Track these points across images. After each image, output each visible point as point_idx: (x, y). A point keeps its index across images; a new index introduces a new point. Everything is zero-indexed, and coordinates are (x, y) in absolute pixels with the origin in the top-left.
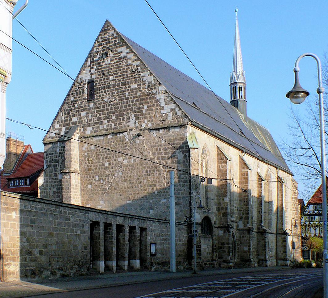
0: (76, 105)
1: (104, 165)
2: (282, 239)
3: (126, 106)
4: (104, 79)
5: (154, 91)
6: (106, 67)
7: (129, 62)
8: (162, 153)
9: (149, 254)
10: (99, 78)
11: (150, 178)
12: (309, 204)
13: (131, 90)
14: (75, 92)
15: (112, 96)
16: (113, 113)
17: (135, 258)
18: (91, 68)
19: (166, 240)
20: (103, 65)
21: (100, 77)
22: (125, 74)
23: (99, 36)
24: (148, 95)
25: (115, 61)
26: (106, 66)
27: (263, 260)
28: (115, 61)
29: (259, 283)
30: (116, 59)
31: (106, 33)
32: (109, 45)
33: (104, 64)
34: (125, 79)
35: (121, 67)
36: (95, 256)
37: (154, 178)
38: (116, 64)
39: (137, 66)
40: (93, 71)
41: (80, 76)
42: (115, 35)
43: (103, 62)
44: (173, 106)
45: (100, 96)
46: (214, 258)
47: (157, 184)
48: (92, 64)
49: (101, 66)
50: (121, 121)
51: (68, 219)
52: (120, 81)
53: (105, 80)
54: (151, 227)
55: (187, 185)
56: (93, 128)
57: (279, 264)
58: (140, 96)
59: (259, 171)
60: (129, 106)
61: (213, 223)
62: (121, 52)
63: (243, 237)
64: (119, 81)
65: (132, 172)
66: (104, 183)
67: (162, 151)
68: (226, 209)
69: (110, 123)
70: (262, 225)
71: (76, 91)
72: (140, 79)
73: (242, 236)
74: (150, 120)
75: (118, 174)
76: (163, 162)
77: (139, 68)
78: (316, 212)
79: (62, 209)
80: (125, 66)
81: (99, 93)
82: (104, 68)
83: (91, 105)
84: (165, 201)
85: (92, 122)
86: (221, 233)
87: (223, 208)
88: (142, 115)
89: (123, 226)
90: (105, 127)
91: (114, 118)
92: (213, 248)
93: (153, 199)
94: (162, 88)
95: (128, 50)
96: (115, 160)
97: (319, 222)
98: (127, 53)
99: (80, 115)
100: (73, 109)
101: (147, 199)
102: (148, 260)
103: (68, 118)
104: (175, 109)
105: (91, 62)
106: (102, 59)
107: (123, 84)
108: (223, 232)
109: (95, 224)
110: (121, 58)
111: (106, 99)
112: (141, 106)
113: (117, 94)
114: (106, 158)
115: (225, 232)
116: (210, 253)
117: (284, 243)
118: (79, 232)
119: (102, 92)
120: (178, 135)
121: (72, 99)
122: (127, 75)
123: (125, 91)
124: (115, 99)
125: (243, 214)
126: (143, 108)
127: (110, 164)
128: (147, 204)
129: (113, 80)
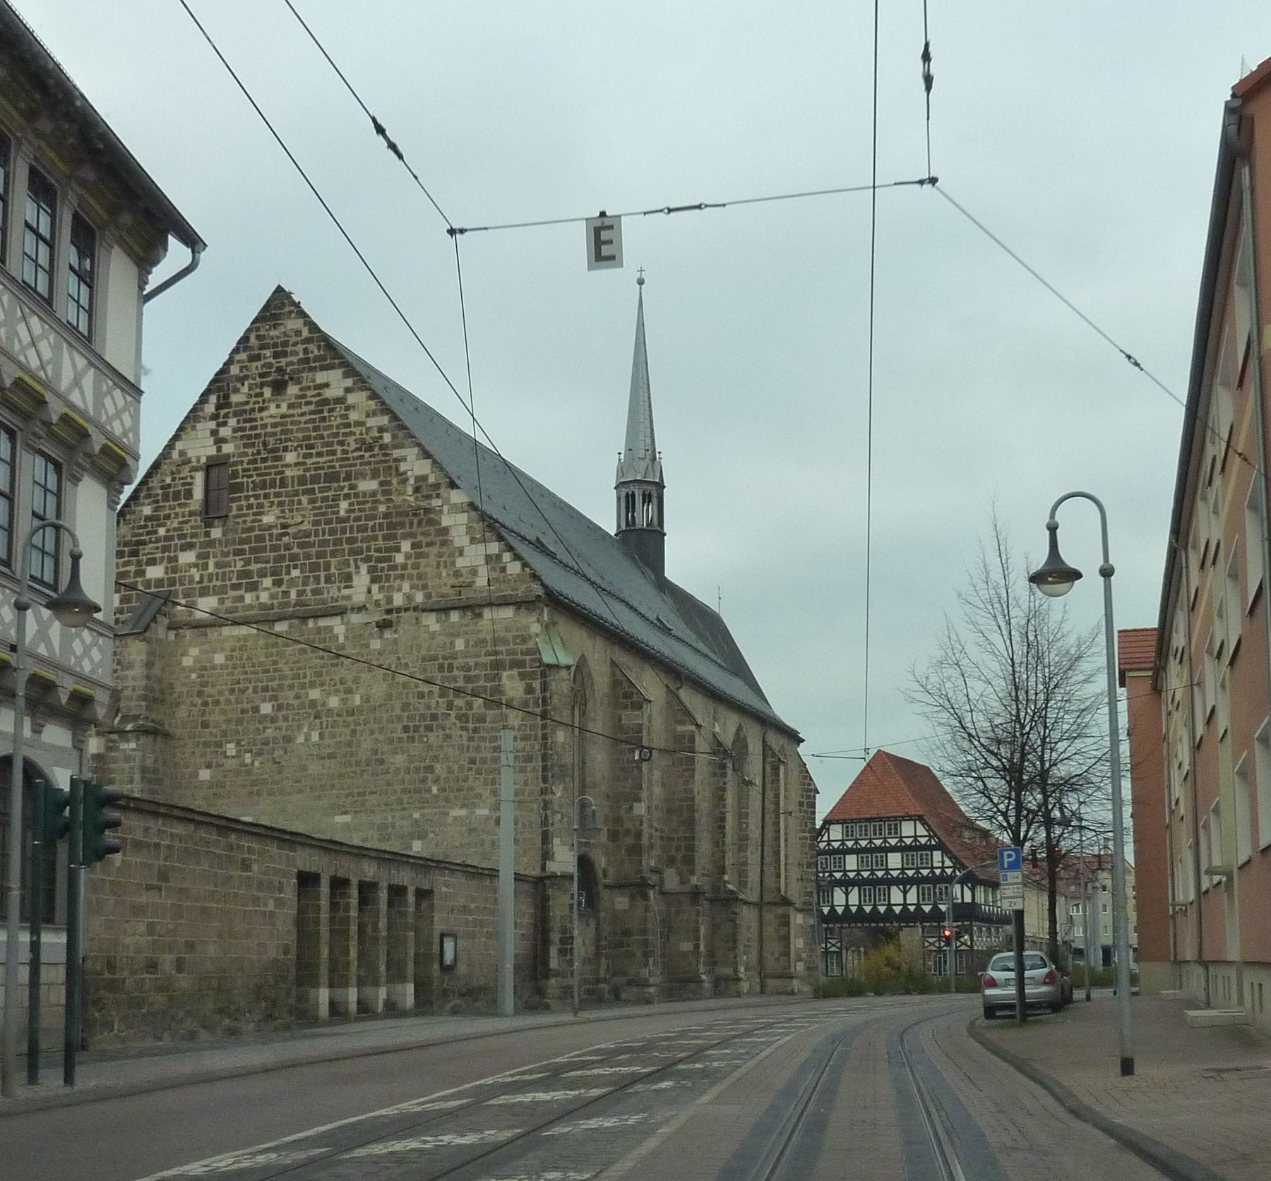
0: (162, 532)
1: (256, 709)
2: (776, 917)
3: (338, 542)
4: (264, 460)
5: (436, 503)
6: (275, 425)
7: (354, 416)
8: (455, 679)
9: (436, 966)
10: (246, 454)
11: (417, 749)
12: (827, 822)
13: (356, 495)
14: (160, 492)
15: (291, 511)
16: (294, 558)
17: (402, 979)
18: (219, 425)
19: (481, 924)
20: (262, 419)
21: (250, 451)
22: (339, 448)
23: (249, 330)
24: (415, 515)
25: (305, 409)
26: (273, 420)
27: (727, 979)
28: (305, 409)
29: (527, 1077)
30: (308, 403)
31: (275, 327)
32: (283, 361)
33: (264, 414)
34: (337, 464)
35: (326, 428)
36: (306, 974)
37: (430, 747)
38: (308, 417)
39: (381, 430)
40: (225, 432)
41: (179, 446)
42: (305, 333)
43: (261, 410)
44: (494, 547)
45: (250, 507)
46: (602, 974)
47: (438, 767)
48: (222, 412)
49: (255, 420)
50: (322, 584)
51: (246, 866)
52: (322, 468)
53: (269, 463)
54: (443, 885)
55: (534, 770)
56: (222, 601)
57: (768, 990)
58: (386, 516)
59: (717, 729)
60: (351, 541)
61: (600, 873)
62: (327, 385)
63: (678, 913)
64: (316, 469)
65: (354, 731)
66: (257, 764)
67: (456, 672)
68: (639, 835)
69: (284, 588)
70: (726, 877)
71: (162, 488)
72: (390, 467)
73: (673, 910)
74: (420, 583)
75: (308, 736)
76: (459, 702)
77: (387, 438)
78: (850, 844)
79: (233, 838)
80: (338, 427)
81: (247, 498)
82: (265, 426)
83: (216, 533)
84: (463, 812)
85: (219, 583)
86: (621, 902)
87: (627, 832)
88: (394, 568)
89: (406, 888)
90: (264, 597)
91: (295, 573)
92: (598, 947)
93: (423, 808)
94: (457, 497)
95: (349, 382)
96: (297, 697)
97: (903, 869)
98: (347, 390)
99: (176, 559)
100: (151, 542)
101: (404, 809)
102: (436, 983)
103: (132, 568)
104: (499, 557)
105: (219, 407)
106: (260, 399)
107: (333, 477)
108: (627, 900)
109: (307, 880)
110: (326, 402)
111: (268, 519)
112: (391, 543)
113: (310, 507)
114: (265, 689)
115: (632, 898)
116: (590, 960)
117: (783, 931)
118: (271, 906)
119: (256, 497)
120: (507, 629)
121: (147, 510)
122: (345, 452)
123: (336, 498)
124: (303, 519)
125: (678, 849)
126: (398, 550)
127: (280, 708)
128: (405, 823)
129: (297, 464)
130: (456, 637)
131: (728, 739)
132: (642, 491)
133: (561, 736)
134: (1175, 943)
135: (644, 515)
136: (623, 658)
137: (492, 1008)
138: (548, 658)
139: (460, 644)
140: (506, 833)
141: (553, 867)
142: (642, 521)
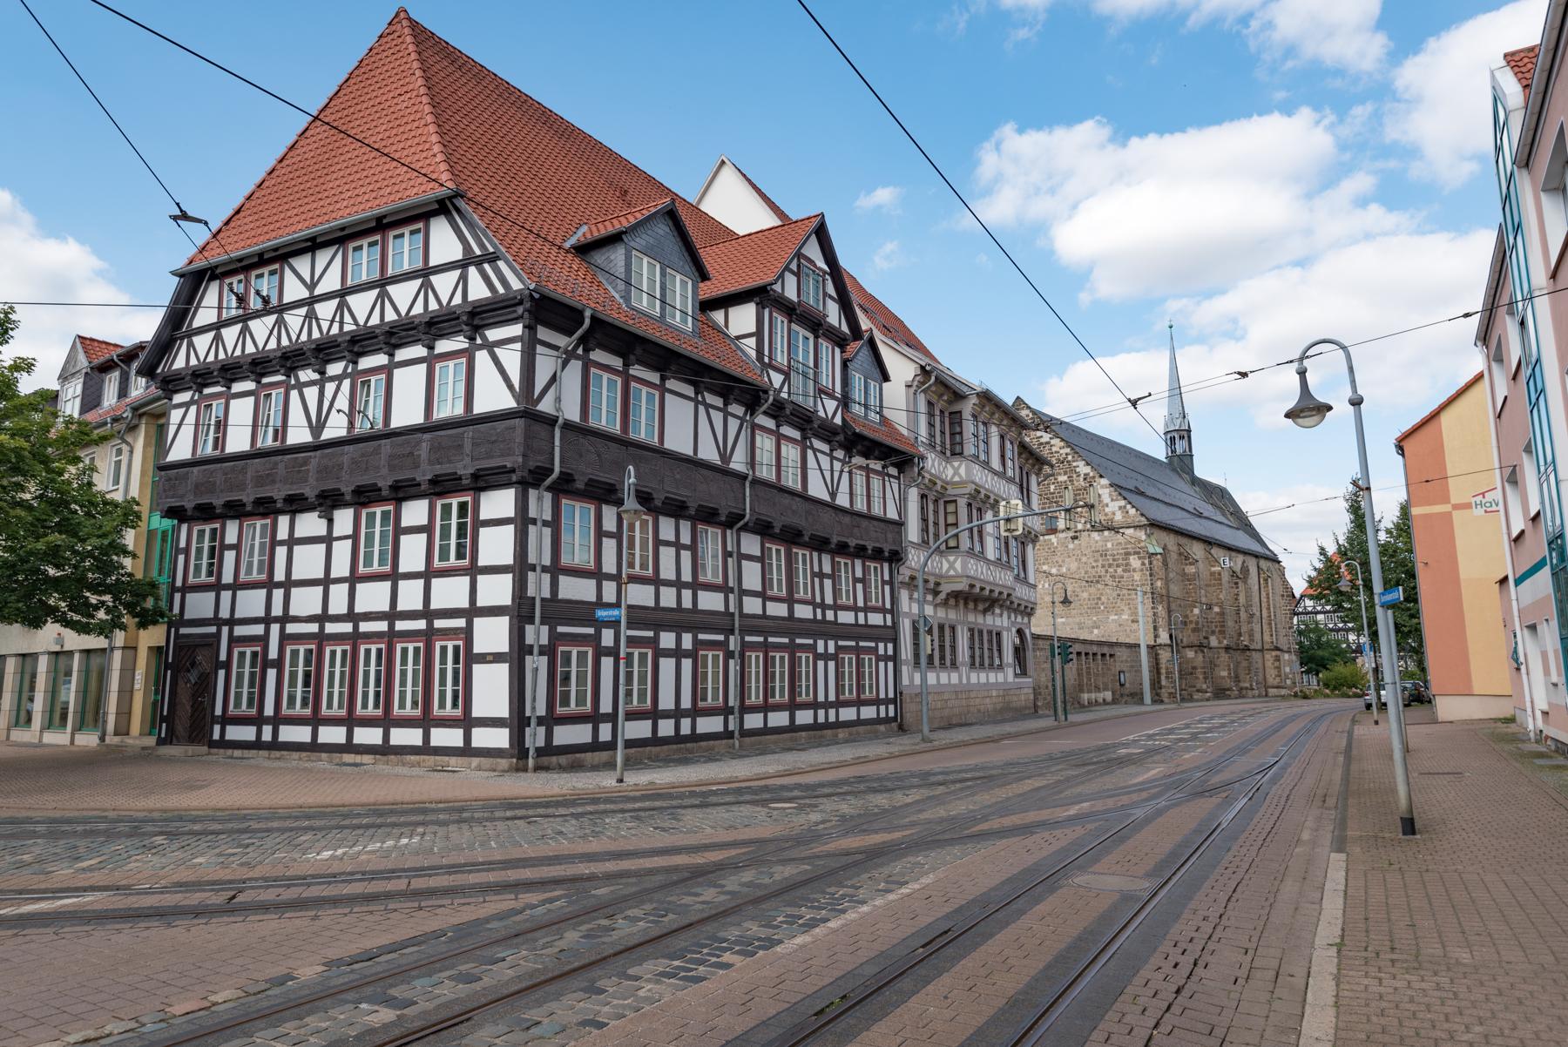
11: (1092, 590)
44: (1123, 503)
130: (1108, 541)
131: (1238, 568)
132: (1179, 436)
133: (1159, 584)
134: (1117, 717)
135: (1180, 447)
136: (1183, 541)
137: (1141, 701)
138: (1151, 550)
139: (1109, 545)
140: (1141, 632)
141: (1159, 641)
142: (1179, 451)
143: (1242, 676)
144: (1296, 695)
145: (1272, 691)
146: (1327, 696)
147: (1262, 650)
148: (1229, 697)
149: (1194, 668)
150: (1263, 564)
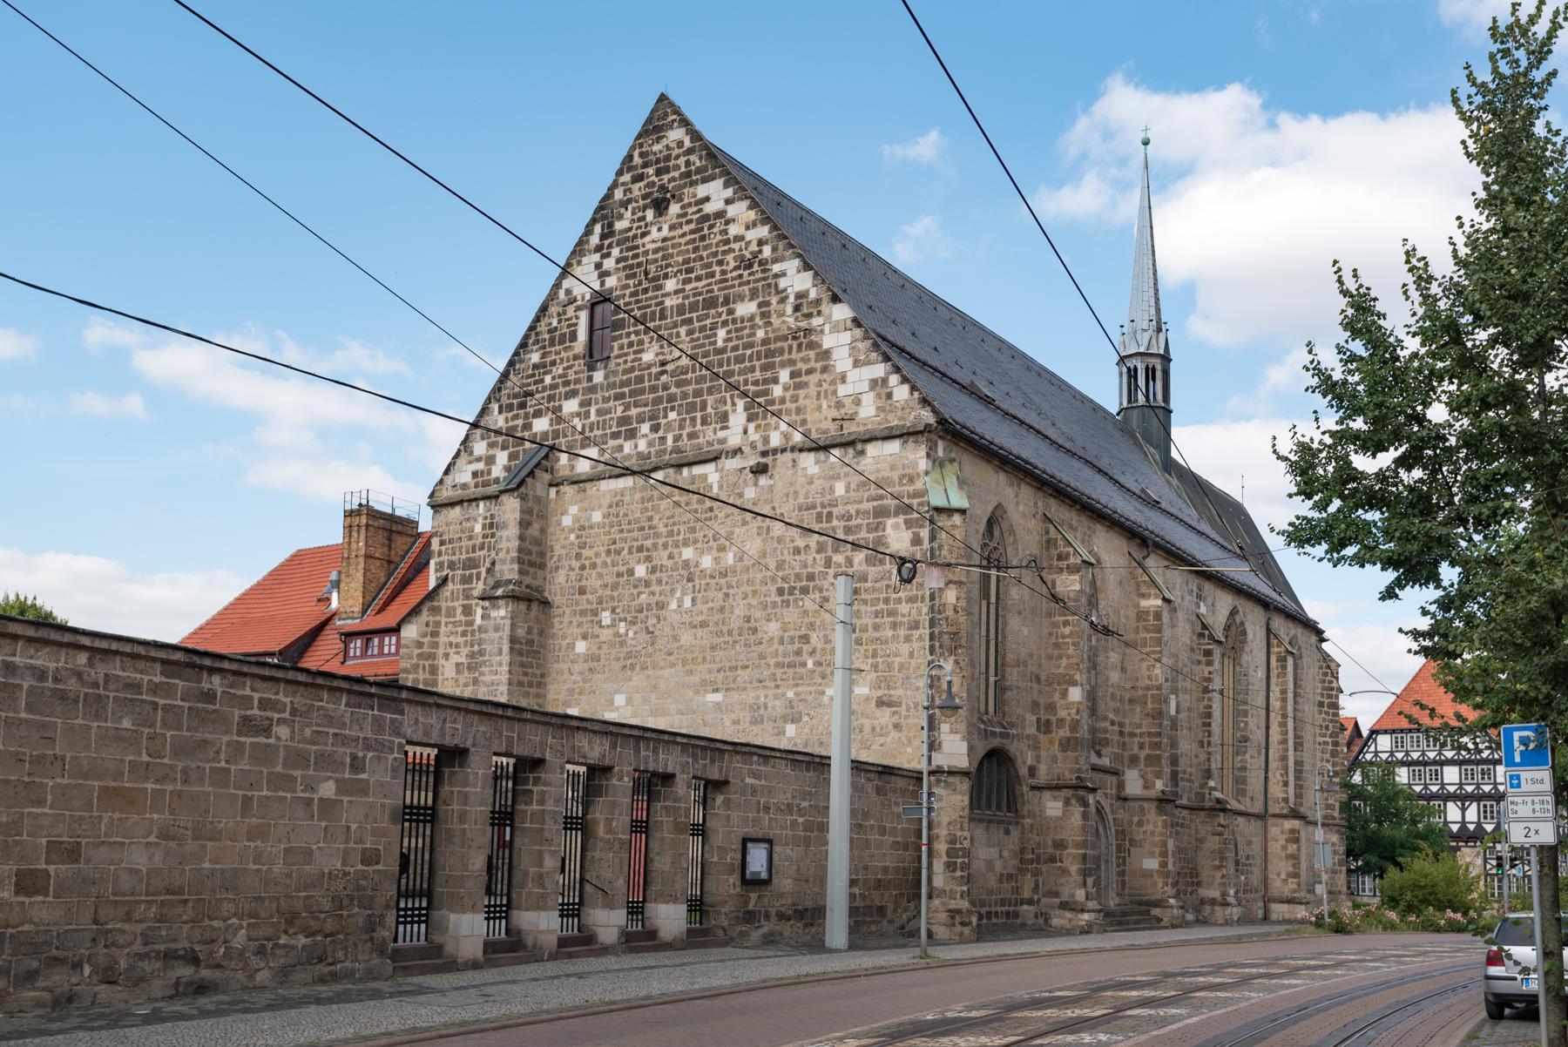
11: (791, 615)
44: (880, 370)
131: (1218, 621)
132: (1149, 373)
139: (840, 489)
141: (940, 760)
143: (1205, 873)
144: (1319, 923)
145: (1278, 910)
146: (1390, 927)
147: (1262, 817)
148: (1156, 924)
149: (1060, 845)
150: (1279, 624)
